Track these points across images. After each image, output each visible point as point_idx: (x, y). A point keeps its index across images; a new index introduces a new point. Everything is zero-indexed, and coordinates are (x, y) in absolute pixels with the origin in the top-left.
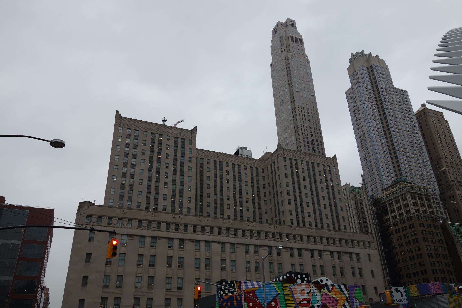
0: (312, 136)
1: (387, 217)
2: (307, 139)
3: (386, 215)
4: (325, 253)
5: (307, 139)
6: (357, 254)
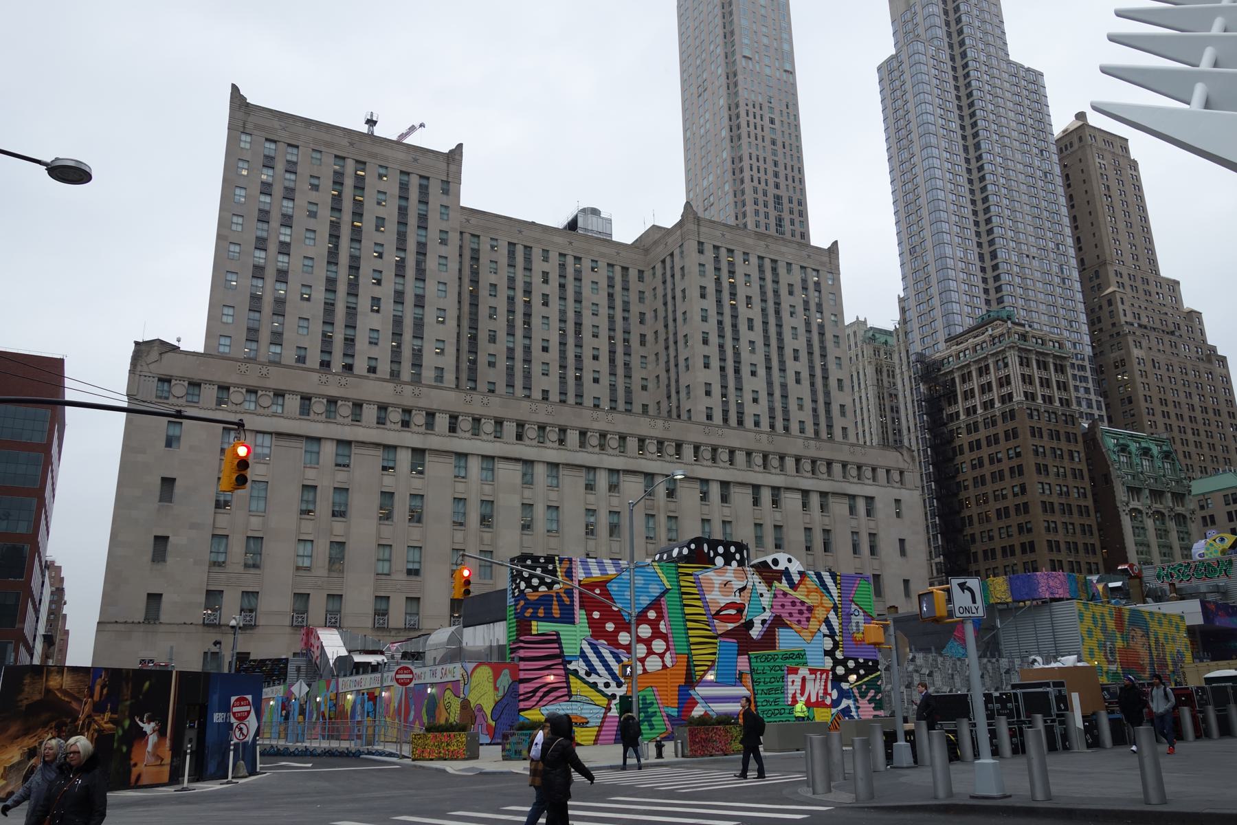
0: (777, 186)
1: (952, 410)
2: (765, 194)
3: (950, 405)
4: (789, 495)
5: (765, 194)
6: (870, 500)
